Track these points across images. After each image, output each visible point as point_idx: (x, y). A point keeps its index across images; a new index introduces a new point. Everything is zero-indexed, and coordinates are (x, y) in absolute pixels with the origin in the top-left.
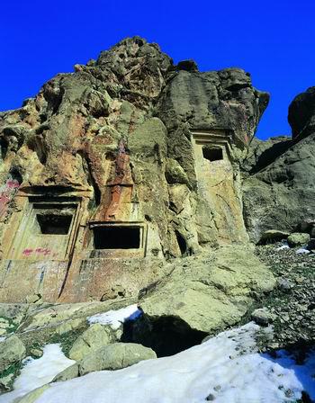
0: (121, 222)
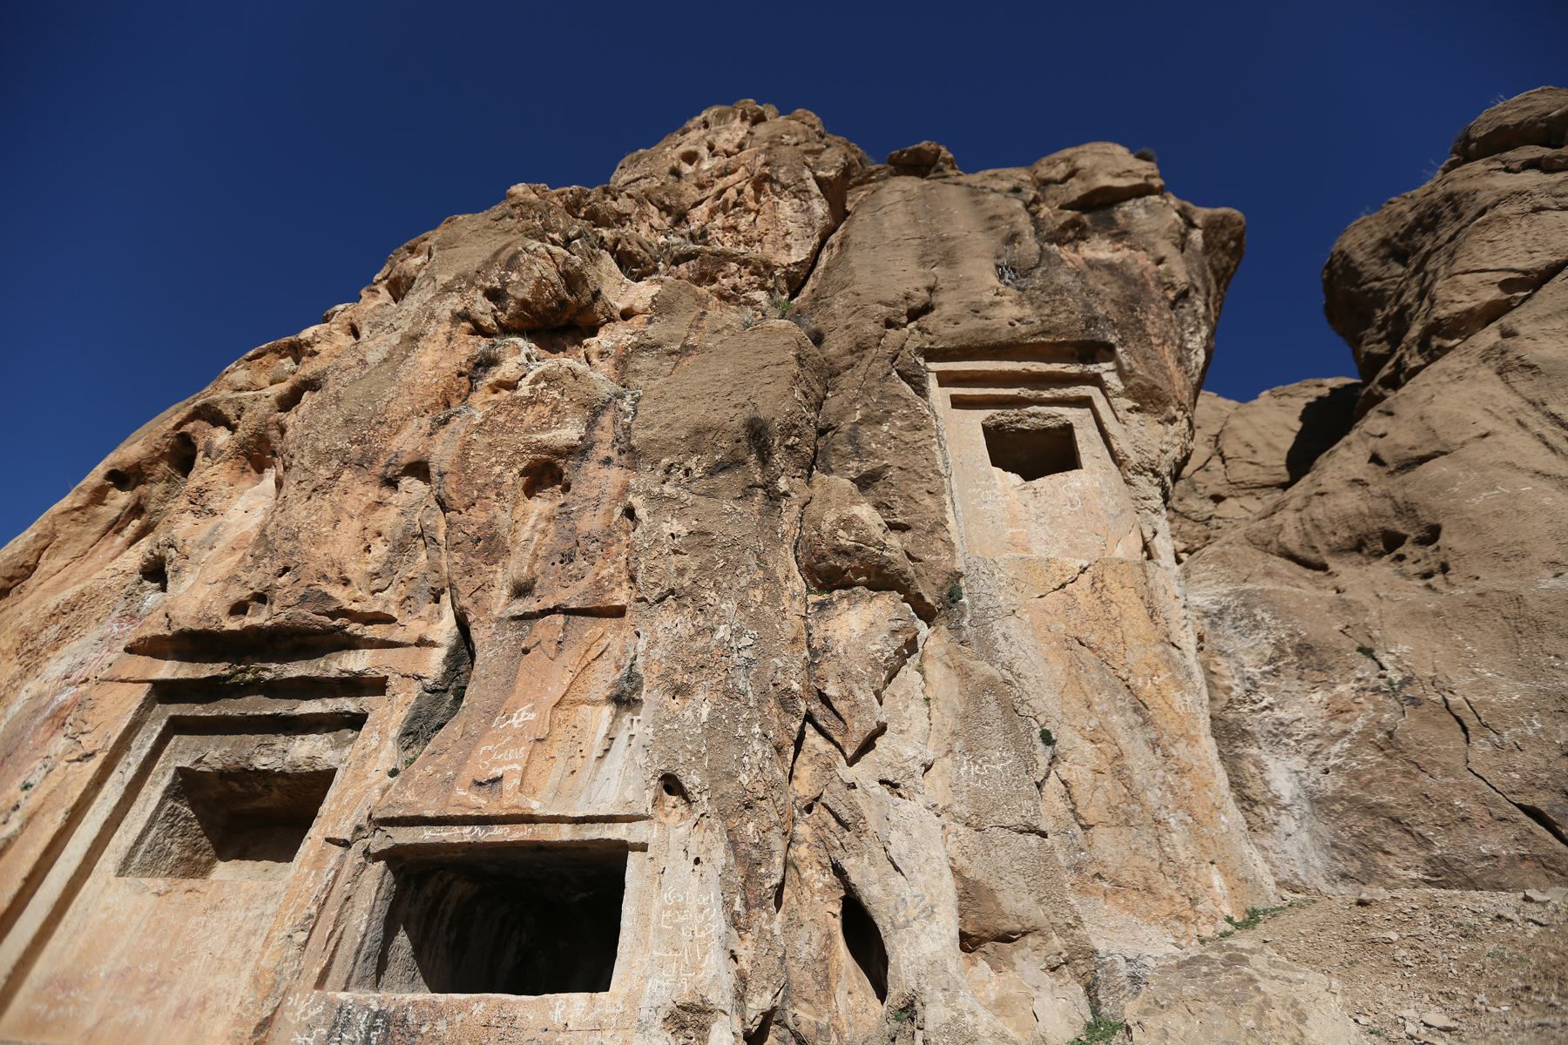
0: (531, 819)
